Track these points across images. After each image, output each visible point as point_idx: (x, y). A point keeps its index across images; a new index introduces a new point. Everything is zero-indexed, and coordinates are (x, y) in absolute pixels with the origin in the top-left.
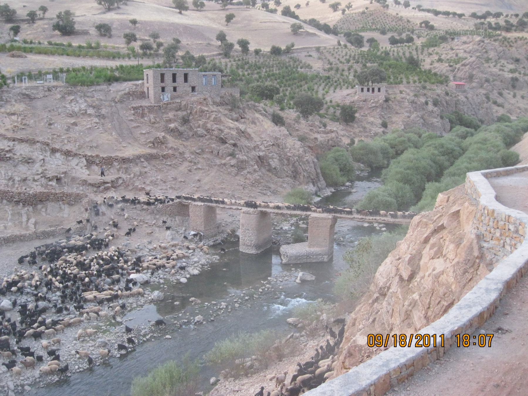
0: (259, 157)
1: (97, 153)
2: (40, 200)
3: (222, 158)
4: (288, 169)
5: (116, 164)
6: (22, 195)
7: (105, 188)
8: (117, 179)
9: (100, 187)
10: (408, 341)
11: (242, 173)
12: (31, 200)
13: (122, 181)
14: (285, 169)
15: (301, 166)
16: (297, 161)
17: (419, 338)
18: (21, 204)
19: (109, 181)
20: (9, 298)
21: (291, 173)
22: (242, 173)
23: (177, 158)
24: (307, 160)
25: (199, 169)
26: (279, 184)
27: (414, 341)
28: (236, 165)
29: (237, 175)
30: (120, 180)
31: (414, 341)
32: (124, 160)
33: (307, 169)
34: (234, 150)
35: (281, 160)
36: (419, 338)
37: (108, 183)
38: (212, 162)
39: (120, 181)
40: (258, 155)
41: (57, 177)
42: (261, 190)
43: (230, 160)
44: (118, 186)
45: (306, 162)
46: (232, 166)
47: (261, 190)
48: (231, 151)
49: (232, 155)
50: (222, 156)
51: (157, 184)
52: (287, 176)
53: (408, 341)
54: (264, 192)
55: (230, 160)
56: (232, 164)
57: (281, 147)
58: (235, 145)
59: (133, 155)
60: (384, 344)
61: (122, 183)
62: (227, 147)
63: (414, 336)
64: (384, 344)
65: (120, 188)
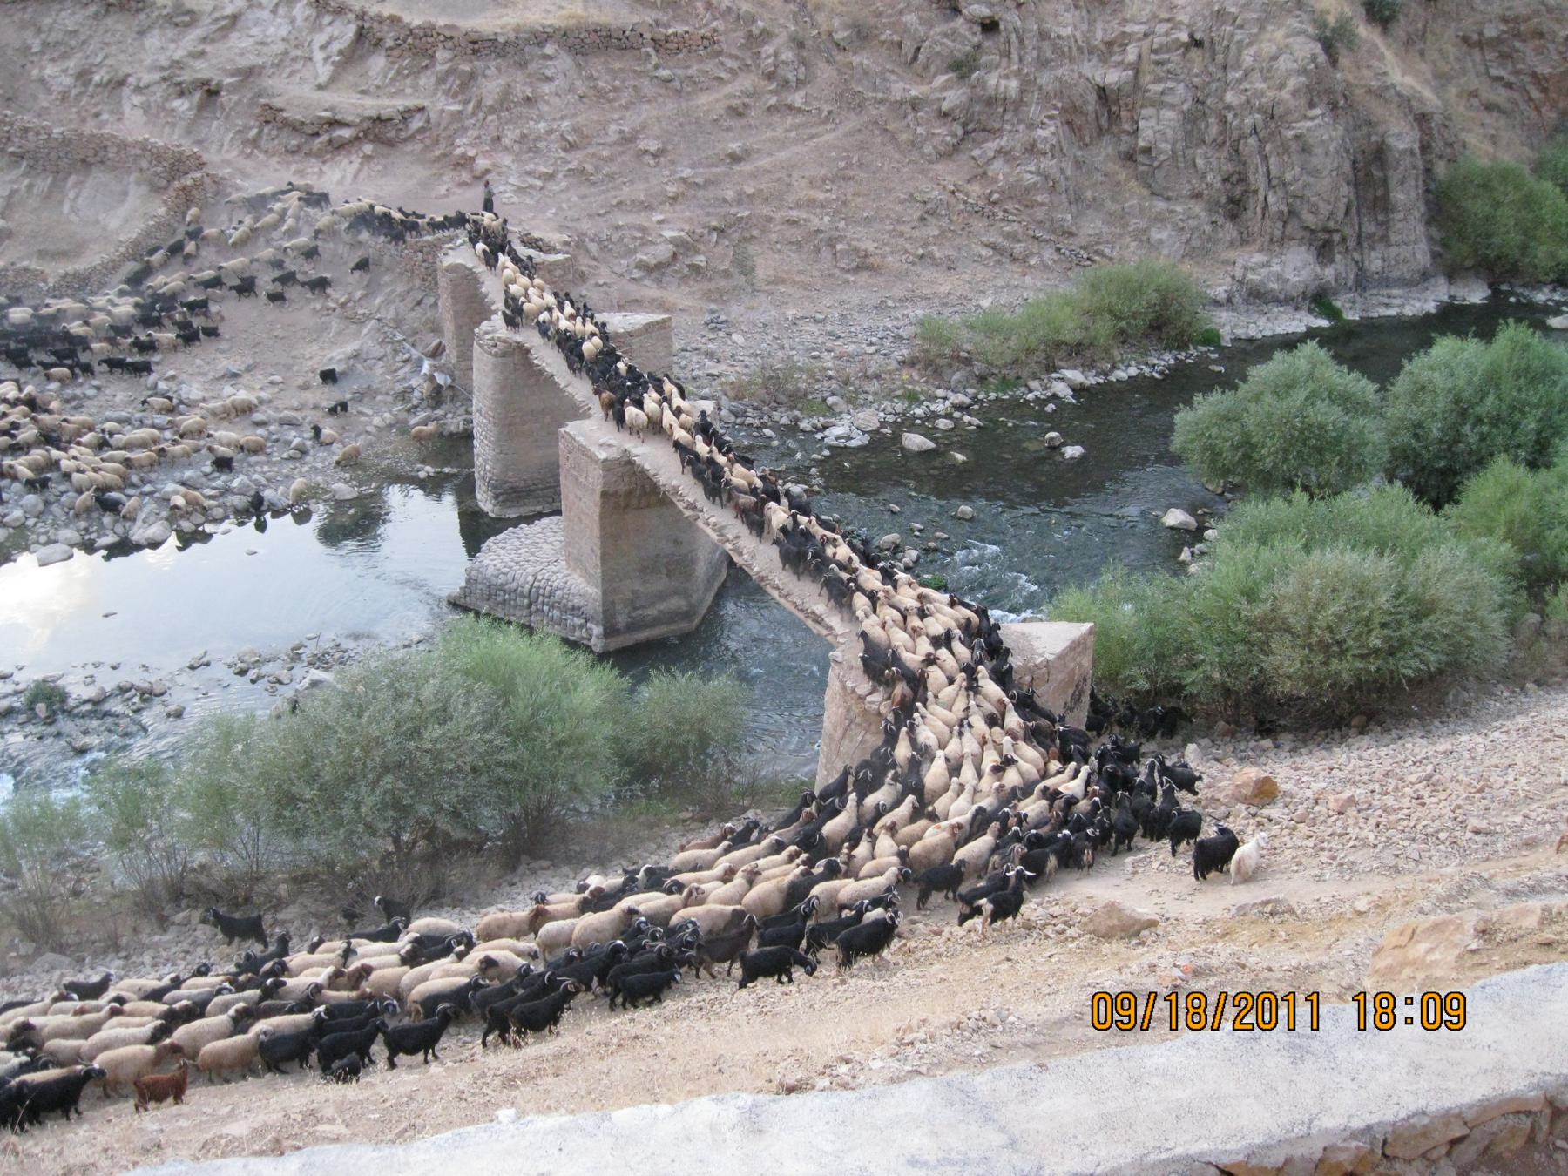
0: (1102, 92)
1: (395, 12)
2: (83, 161)
3: (923, 76)
4: (1211, 166)
5: (441, 55)
6: (31, 135)
7: (330, 141)
8: (407, 115)
9: (317, 134)
10: (1210, 1011)
11: (976, 153)
12: (53, 155)
13: (421, 124)
14: (1200, 162)
15: (1265, 158)
16: (1255, 130)
17: (1243, 1003)
18: (24, 164)
19: (349, 119)
20: (1089, 643)
21: (1217, 183)
22: (976, 153)
23: (720, 53)
24: (1297, 137)
25: (791, 107)
26: (1136, 223)
27: (1230, 1012)
28: (957, 113)
29: (949, 153)
30: (418, 116)
31: (1230, 1012)
32: (478, 46)
33: (1288, 177)
34: (978, 47)
35: (1192, 119)
36: (1243, 1003)
37: (347, 125)
38: (875, 89)
39: (417, 123)
40: (1098, 80)
41: (205, 83)
42: (1008, 236)
43: (945, 88)
44: (405, 140)
45: (1294, 147)
46: (946, 115)
47: (1008, 236)
48: (961, 49)
49: (962, 68)
50: (926, 68)
51: (536, 151)
52: (1197, 196)
53: (1210, 1011)
54: (1018, 248)
55: (945, 88)
56: (945, 106)
57: (1220, 58)
58: (990, 26)
59: (517, 29)
60: (1210, 1019)
61: (421, 130)
62: (954, 31)
63: (1230, 999)
64: (1210, 1019)
65: (409, 147)
